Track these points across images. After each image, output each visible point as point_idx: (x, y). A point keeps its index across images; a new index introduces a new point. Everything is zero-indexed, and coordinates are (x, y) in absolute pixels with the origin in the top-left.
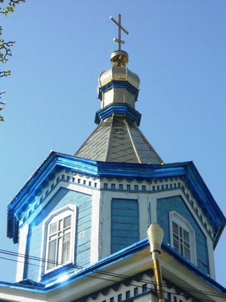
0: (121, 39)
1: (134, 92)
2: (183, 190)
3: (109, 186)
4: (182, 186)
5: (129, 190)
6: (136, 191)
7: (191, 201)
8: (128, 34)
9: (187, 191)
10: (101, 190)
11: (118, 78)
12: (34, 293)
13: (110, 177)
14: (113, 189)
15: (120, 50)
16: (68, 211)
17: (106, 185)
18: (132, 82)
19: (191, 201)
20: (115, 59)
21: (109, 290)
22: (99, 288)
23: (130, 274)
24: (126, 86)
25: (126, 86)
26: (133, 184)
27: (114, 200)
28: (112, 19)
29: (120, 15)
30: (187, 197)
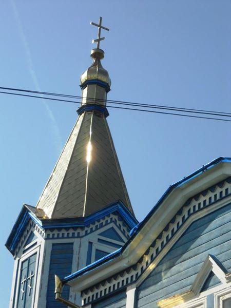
0: (100, 41)
1: (106, 87)
2: (115, 222)
3: (51, 236)
4: (115, 219)
5: (68, 237)
6: (73, 237)
7: (122, 230)
8: (108, 30)
9: (119, 223)
10: (45, 239)
11: (94, 76)
12: (172, 194)
13: (52, 230)
14: (53, 238)
15: (98, 48)
16: (24, 264)
17: (48, 235)
18: (104, 79)
19: (122, 230)
20: (94, 56)
21: (215, 187)
22: (215, 182)
23: (204, 188)
24: (99, 84)
25: (99, 84)
26: (71, 232)
27: (53, 245)
28: (93, 24)
29: (101, 18)
30: (119, 227)
